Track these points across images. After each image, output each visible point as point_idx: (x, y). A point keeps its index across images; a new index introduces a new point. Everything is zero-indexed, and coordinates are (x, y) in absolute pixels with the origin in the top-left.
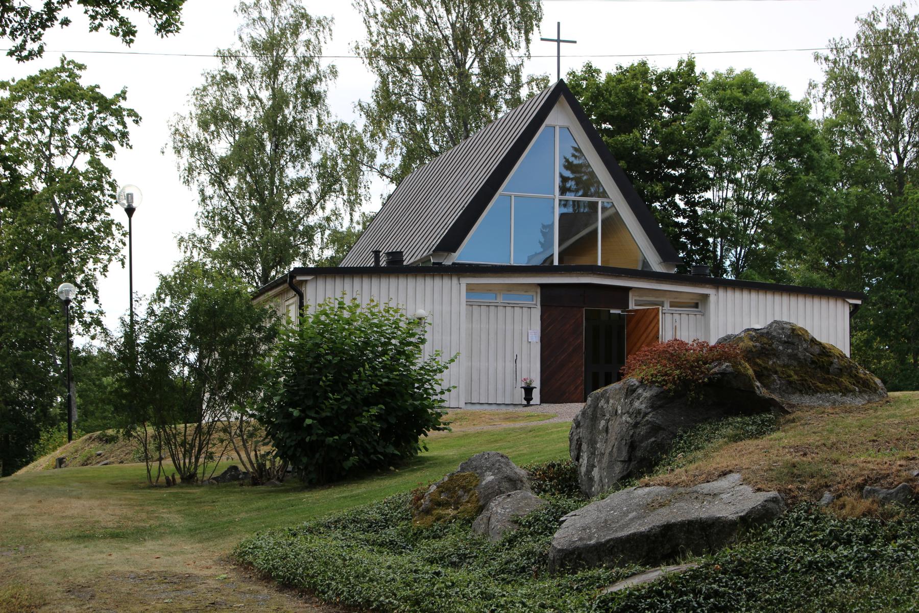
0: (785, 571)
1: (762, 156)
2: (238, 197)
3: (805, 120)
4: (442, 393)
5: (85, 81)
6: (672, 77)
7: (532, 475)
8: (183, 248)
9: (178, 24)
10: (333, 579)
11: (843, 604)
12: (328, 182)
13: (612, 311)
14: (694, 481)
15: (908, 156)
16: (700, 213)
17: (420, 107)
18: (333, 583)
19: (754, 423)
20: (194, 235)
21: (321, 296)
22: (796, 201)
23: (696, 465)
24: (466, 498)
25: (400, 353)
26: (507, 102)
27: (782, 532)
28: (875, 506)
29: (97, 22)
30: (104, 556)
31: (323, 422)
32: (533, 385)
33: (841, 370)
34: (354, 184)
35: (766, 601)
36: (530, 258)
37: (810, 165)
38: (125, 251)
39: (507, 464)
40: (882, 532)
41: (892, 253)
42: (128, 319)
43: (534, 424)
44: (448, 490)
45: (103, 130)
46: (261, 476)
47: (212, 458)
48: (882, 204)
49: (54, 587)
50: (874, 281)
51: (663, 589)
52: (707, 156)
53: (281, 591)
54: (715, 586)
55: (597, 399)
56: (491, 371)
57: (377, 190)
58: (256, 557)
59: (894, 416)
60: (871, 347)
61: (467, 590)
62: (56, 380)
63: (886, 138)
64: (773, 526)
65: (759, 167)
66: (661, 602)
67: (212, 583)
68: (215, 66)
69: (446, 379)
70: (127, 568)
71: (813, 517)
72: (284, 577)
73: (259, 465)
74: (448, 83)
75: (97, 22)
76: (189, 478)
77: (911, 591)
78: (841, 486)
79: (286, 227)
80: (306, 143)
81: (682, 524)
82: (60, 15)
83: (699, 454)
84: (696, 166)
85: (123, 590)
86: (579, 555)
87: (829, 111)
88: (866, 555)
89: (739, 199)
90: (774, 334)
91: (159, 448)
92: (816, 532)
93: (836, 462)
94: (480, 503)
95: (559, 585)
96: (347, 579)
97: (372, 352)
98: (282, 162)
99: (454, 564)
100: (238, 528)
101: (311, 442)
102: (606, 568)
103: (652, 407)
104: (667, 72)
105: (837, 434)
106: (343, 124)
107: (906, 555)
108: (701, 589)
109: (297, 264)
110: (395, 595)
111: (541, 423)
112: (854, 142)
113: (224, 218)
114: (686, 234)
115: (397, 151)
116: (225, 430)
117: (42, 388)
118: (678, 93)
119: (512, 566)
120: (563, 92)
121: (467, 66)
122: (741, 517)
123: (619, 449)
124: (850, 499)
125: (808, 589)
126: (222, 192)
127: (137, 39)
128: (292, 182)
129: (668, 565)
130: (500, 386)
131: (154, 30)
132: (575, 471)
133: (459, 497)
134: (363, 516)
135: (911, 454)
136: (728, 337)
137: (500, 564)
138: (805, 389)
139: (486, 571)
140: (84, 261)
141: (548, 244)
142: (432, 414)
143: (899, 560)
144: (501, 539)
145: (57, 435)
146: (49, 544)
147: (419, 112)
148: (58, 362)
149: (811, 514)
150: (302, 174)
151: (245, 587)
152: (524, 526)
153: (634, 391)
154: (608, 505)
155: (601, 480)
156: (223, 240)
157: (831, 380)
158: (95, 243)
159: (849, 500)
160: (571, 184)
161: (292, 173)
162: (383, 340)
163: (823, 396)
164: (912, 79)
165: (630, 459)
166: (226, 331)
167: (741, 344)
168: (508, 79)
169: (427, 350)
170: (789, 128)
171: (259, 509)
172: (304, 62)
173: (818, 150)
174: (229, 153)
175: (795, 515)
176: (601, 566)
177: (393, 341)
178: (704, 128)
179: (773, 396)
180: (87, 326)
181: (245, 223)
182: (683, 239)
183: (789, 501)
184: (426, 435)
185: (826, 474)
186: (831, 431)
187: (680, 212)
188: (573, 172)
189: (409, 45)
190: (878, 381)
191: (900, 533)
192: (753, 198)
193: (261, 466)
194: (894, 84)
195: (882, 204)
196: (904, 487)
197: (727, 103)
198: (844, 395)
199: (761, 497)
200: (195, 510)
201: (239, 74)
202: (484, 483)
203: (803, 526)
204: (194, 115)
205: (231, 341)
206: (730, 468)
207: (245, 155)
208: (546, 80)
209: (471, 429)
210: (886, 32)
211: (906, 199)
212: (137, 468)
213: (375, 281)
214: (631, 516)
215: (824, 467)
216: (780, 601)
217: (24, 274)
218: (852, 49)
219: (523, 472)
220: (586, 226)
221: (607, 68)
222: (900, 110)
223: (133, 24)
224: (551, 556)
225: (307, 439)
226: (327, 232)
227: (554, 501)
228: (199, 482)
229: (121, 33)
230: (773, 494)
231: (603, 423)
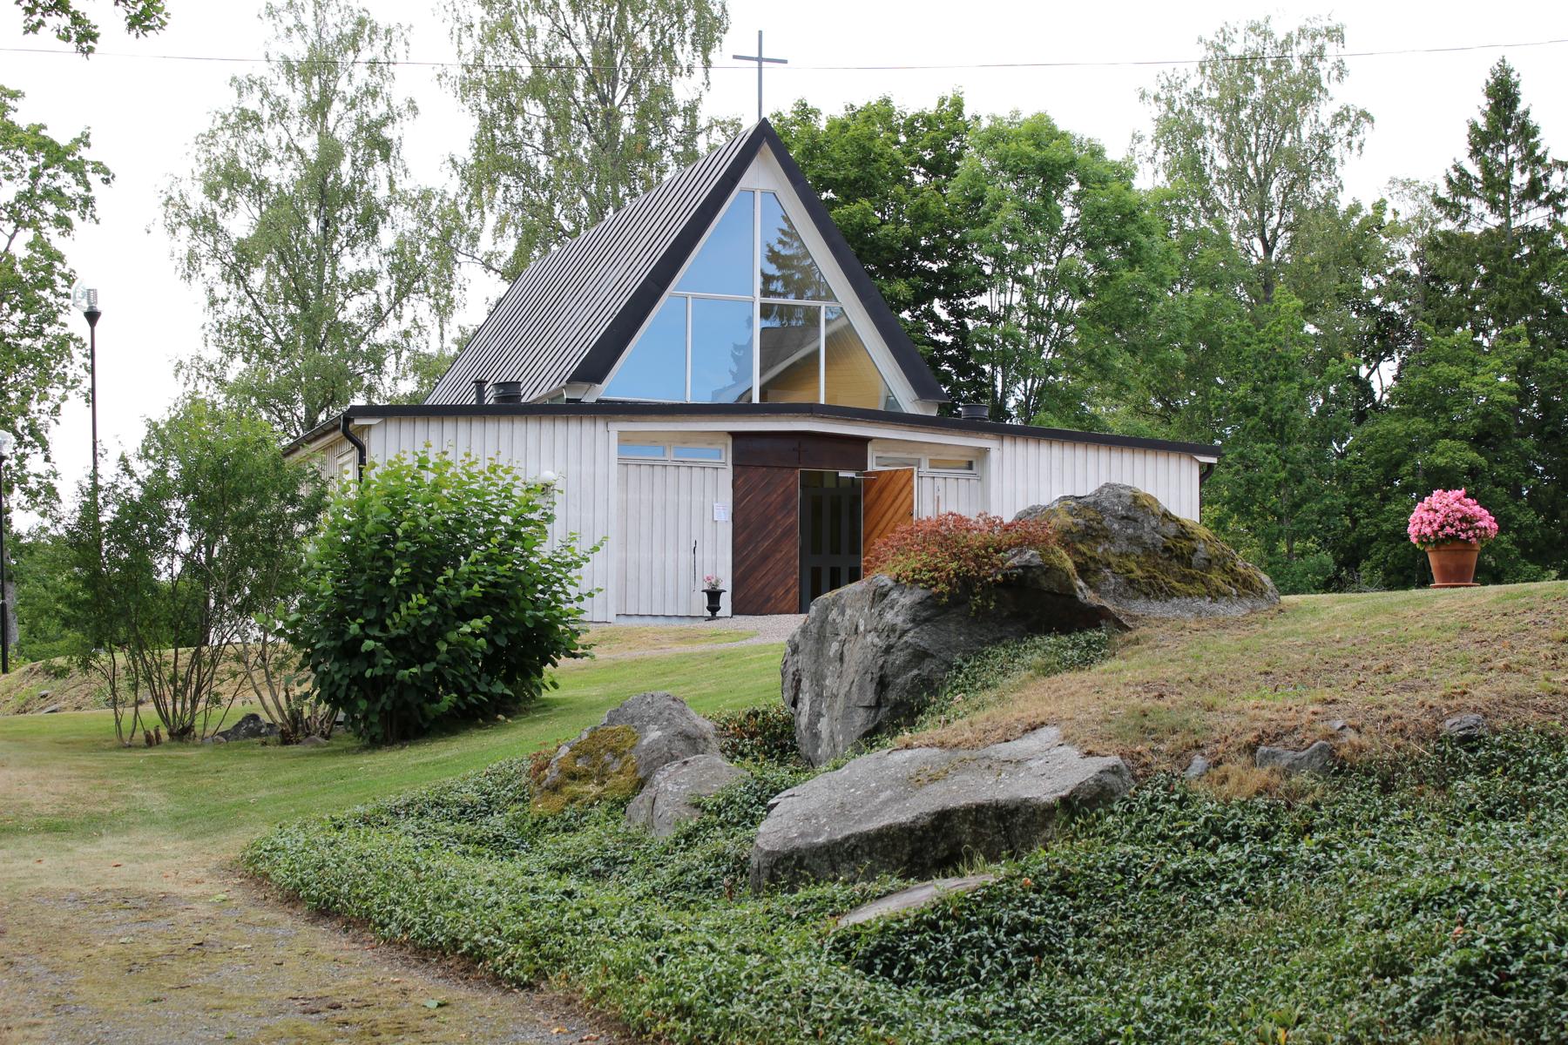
0: (1135, 888)
2: (267, 301)
3: (1129, 188)
4: (580, 598)
6: (928, 121)
8: (182, 378)
9: (162, 16)
10: (398, 903)
12: (407, 277)
13: (841, 474)
14: (984, 739)
15: (1279, 244)
16: (971, 327)
17: (542, 164)
18: (399, 910)
19: (1075, 645)
20: (200, 358)
21: (391, 447)
22: (1115, 314)
23: (987, 713)
25: (514, 535)
27: (1128, 822)
28: (1276, 779)
29: (36, 19)
30: (30, 862)
31: (392, 644)
32: (720, 588)
33: (1210, 561)
35: (1107, 936)
36: (716, 394)
37: (1134, 258)
39: (682, 712)
40: (1289, 820)
42: (87, 483)
43: (722, 646)
46: (295, 730)
47: (218, 701)
50: (1228, 431)
51: (939, 918)
53: (313, 922)
54: (1024, 913)
55: (826, 609)
56: (657, 565)
57: (478, 291)
59: (1294, 633)
60: (1224, 530)
61: (618, 922)
63: (1246, 217)
64: (1113, 812)
65: (1059, 259)
66: (936, 940)
67: (202, 909)
68: (228, 101)
69: (586, 578)
70: (65, 884)
71: (1177, 797)
75: (36, 19)
76: (182, 734)
77: (1342, 920)
78: (1221, 747)
80: (370, 220)
81: (967, 810)
83: (990, 695)
85: (54, 921)
86: (801, 859)
87: (1162, 176)
88: (1265, 859)
89: (1031, 309)
90: (1106, 504)
91: (135, 687)
92: (1182, 822)
93: (1210, 709)
94: (641, 775)
95: (768, 912)
96: (422, 903)
97: (470, 536)
98: (335, 246)
99: (596, 874)
100: (253, 815)
101: (374, 678)
103: (913, 620)
105: (1208, 663)
106: (428, 191)
107: (1330, 858)
108: (1001, 918)
109: (359, 400)
110: (500, 930)
111: (734, 646)
113: (246, 332)
114: (950, 360)
116: (239, 658)
118: (937, 146)
119: (690, 878)
120: (764, 136)
123: (861, 688)
125: (1175, 916)
126: (242, 292)
127: (99, 46)
130: (670, 589)
131: (125, 25)
132: (789, 723)
133: (605, 765)
134: (451, 797)
135: (1328, 694)
137: (671, 874)
138: (1154, 590)
139: (647, 886)
140: (26, 396)
141: (743, 373)
142: (564, 632)
143: (1318, 868)
144: (674, 834)
149: (1174, 792)
150: (365, 265)
151: (256, 915)
152: (709, 812)
153: (885, 595)
154: (845, 779)
155: (832, 737)
156: (245, 365)
157: (1194, 578)
159: (1234, 768)
160: (777, 286)
161: (349, 264)
162: (486, 516)
163: (1184, 601)
165: (878, 705)
166: (240, 503)
167: (1054, 521)
168: (678, 122)
169: (557, 531)
170: (1103, 201)
171: (288, 784)
172: (367, 92)
173: (1149, 234)
174: (252, 233)
175: (1149, 795)
176: (835, 880)
177: (503, 519)
178: (978, 199)
179: (1104, 603)
181: (278, 340)
182: (945, 367)
183: (1139, 772)
184: (555, 665)
185: (1197, 728)
186: (1198, 658)
187: (941, 326)
188: (780, 268)
189: (526, 72)
190: (1265, 578)
191: (1317, 822)
193: (296, 717)
194: (1258, 136)
196: (1322, 748)
197: (1011, 162)
198: (1215, 600)
199: (1094, 766)
200: (188, 785)
201: (266, 114)
202: (645, 742)
203: (1161, 812)
204: (197, 175)
205: (251, 518)
206: (1042, 718)
207: (276, 235)
208: (736, 124)
209: (625, 655)
210: (1242, 59)
211: (1277, 309)
212: (100, 717)
215: (1192, 716)
216: (1129, 936)
219: (708, 726)
220: (800, 346)
221: (831, 107)
223: (93, 23)
224: (754, 861)
225: (368, 673)
226: (405, 354)
227: (757, 772)
228: (198, 740)
229: (74, 37)
230: (1113, 760)
231: (835, 646)
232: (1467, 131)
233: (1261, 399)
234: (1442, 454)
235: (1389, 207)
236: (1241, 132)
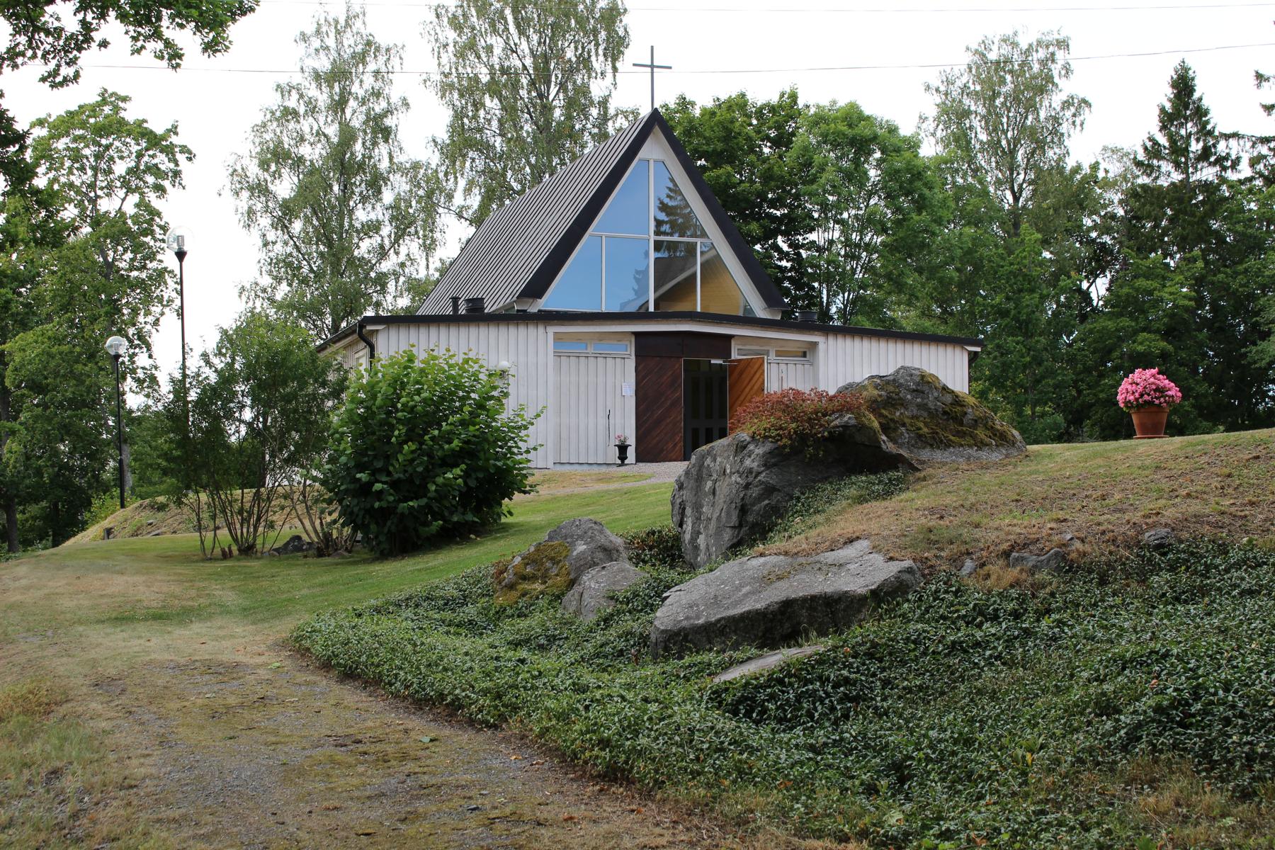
0: (924, 654)
1: (870, 195)
3: (916, 156)
4: (528, 452)
5: (130, 114)
6: (773, 109)
7: (629, 544)
8: (244, 298)
10: (401, 669)
11: (994, 692)
12: (403, 223)
14: (816, 549)
15: (1024, 194)
17: (498, 142)
18: (402, 673)
19: (880, 482)
20: (257, 284)
21: (391, 345)
22: (906, 244)
23: (818, 531)
24: (555, 571)
26: (593, 136)
27: (919, 607)
28: (1024, 576)
29: (139, 44)
30: (142, 641)
31: (395, 485)
34: (430, 225)
35: (904, 688)
38: (178, 302)
39: (601, 532)
40: (1033, 605)
41: (1008, 298)
43: (630, 485)
44: (534, 561)
45: (154, 170)
46: (327, 547)
48: (996, 246)
49: (80, 681)
52: (811, 195)
54: (845, 673)
55: (703, 457)
57: (454, 234)
58: (314, 642)
59: (1036, 472)
61: (557, 681)
62: (107, 443)
64: (908, 601)
65: (867, 206)
66: (783, 692)
68: (274, 101)
69: (533, 436)
70: (167, 656)
72: (345, 666)
73: (324, 534)
74: (530, 126)
75: (139, 44)
76: (248, 550)
78: (984, 553)
79: (357, 274)
80: (376, 183)
81: (804, 600)
82: (97, 36)
84: (799, 206)
85: (160, 682)
86: (686, 636)
89: (848, 243)
90: (902, 381)
91: (214, 517)
93: (977, 526)
94: (571, 577)
96: (418, 668)
101: (381, 508)
102: (718, 652)
103: (765, 465)
104: (767, 105)
105: (975, 494)
109: (370, 313)
112: (965, 180)
113: (289, 265)
114: (790, 279)
115: (476, 190)
117: (91, 449)
118: (779, 127)
119: (608, 649)
120: (656, 121)
121: (551, 98)
122: (872, 591)
123: (728, 513)
124: (995, 568)
125: (952, 673)
126: (286, 237)
127: (184, 63)
128: (363, 226)
129: (789, 647)
130: (592, 445)
132: (677, 539)
135: (1061, 515)
136: (850, 386)
138: (936, 442)
139: (577, 655)
140: (135, 311)
141: (643, 290)
144: (596, 618)
145: (109, 502)
146: (81, 629)
147: (498, 149)
148: (111, 423)
149: (952, 586)
150: (373, 216)
151: (302, 677)
153: (745, 447)
154: (717, 578)
155: (708, 549)
158: (148, 289)
161: (362, 215)
162: (461, 393)
164: (1027, 112)
165: (740, 526)
168: (594, 112)
169: (511, 404)
171: (322, 585)
172: (373, 94)
173: (931, 188)
175: (934, 588)
176: (710, 650)
177: (473, 395)
178: (809, 164)
179: (901, 452)
180: (140, 382)
181: (311, 270)
182: (786, 284)
186: (968, 490)
187: (783, 255)
188: (668, 215)
189: (485, 78)
190: (1016, 433)
191: (1054, 606)
192: (861, 239)
193: (327, 536)
194: (1008, 117)
195: (996, 246)
196: (1057, 554)
197: (831, 138)
198: (980, 449)
199: (894, 567)
203: (943, 600)
209: (561, 492)
210: (998, 63)
211: (1023, 241)
212: (190, 539)
213: (453, 330)
214: (744, 590)
216: (920, 688)
217: (70, 327)
218: (964, 79)
219: (619, 541)
220: (683, 270)
221: (703, 99)
222: (1015, 146)
224: (653, 637)
226: (402, 279)
227: (655, 574)
230: (908, 563)
231: (709, 484)
232: (1158, 112)
233: (1011, 305)
234: (1141, 343)
235: (1102, 167)
236: (997, 115)
